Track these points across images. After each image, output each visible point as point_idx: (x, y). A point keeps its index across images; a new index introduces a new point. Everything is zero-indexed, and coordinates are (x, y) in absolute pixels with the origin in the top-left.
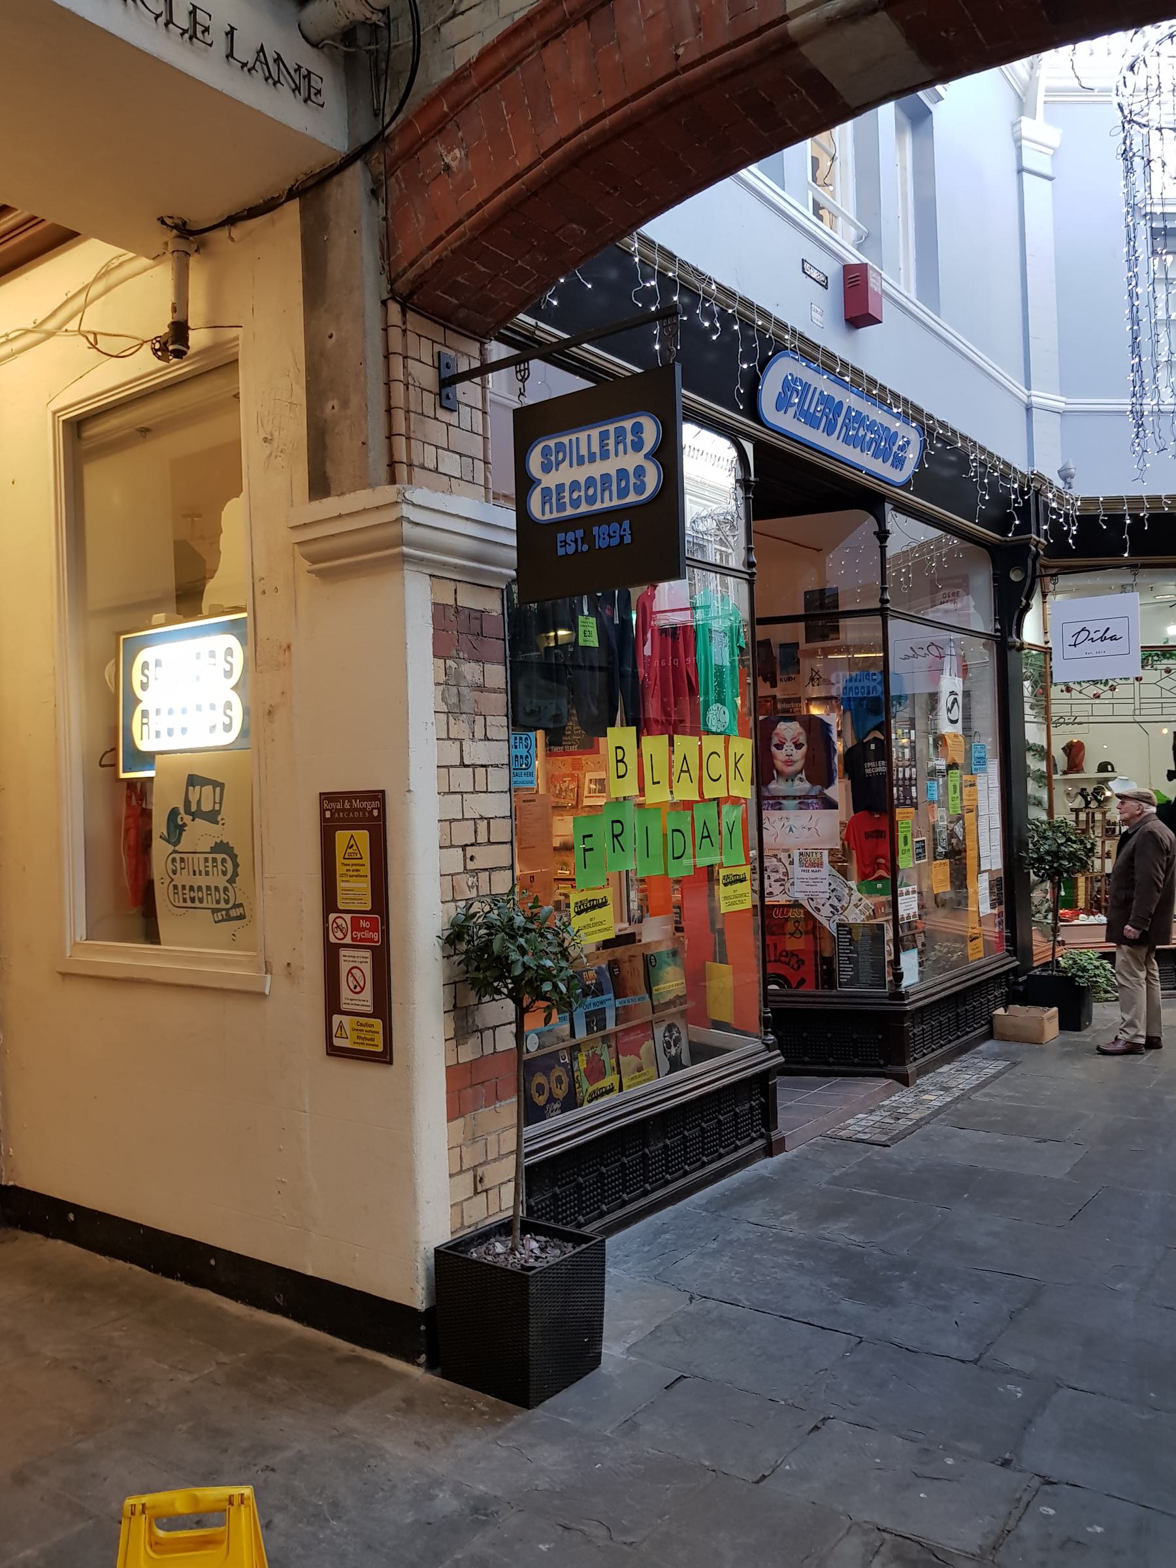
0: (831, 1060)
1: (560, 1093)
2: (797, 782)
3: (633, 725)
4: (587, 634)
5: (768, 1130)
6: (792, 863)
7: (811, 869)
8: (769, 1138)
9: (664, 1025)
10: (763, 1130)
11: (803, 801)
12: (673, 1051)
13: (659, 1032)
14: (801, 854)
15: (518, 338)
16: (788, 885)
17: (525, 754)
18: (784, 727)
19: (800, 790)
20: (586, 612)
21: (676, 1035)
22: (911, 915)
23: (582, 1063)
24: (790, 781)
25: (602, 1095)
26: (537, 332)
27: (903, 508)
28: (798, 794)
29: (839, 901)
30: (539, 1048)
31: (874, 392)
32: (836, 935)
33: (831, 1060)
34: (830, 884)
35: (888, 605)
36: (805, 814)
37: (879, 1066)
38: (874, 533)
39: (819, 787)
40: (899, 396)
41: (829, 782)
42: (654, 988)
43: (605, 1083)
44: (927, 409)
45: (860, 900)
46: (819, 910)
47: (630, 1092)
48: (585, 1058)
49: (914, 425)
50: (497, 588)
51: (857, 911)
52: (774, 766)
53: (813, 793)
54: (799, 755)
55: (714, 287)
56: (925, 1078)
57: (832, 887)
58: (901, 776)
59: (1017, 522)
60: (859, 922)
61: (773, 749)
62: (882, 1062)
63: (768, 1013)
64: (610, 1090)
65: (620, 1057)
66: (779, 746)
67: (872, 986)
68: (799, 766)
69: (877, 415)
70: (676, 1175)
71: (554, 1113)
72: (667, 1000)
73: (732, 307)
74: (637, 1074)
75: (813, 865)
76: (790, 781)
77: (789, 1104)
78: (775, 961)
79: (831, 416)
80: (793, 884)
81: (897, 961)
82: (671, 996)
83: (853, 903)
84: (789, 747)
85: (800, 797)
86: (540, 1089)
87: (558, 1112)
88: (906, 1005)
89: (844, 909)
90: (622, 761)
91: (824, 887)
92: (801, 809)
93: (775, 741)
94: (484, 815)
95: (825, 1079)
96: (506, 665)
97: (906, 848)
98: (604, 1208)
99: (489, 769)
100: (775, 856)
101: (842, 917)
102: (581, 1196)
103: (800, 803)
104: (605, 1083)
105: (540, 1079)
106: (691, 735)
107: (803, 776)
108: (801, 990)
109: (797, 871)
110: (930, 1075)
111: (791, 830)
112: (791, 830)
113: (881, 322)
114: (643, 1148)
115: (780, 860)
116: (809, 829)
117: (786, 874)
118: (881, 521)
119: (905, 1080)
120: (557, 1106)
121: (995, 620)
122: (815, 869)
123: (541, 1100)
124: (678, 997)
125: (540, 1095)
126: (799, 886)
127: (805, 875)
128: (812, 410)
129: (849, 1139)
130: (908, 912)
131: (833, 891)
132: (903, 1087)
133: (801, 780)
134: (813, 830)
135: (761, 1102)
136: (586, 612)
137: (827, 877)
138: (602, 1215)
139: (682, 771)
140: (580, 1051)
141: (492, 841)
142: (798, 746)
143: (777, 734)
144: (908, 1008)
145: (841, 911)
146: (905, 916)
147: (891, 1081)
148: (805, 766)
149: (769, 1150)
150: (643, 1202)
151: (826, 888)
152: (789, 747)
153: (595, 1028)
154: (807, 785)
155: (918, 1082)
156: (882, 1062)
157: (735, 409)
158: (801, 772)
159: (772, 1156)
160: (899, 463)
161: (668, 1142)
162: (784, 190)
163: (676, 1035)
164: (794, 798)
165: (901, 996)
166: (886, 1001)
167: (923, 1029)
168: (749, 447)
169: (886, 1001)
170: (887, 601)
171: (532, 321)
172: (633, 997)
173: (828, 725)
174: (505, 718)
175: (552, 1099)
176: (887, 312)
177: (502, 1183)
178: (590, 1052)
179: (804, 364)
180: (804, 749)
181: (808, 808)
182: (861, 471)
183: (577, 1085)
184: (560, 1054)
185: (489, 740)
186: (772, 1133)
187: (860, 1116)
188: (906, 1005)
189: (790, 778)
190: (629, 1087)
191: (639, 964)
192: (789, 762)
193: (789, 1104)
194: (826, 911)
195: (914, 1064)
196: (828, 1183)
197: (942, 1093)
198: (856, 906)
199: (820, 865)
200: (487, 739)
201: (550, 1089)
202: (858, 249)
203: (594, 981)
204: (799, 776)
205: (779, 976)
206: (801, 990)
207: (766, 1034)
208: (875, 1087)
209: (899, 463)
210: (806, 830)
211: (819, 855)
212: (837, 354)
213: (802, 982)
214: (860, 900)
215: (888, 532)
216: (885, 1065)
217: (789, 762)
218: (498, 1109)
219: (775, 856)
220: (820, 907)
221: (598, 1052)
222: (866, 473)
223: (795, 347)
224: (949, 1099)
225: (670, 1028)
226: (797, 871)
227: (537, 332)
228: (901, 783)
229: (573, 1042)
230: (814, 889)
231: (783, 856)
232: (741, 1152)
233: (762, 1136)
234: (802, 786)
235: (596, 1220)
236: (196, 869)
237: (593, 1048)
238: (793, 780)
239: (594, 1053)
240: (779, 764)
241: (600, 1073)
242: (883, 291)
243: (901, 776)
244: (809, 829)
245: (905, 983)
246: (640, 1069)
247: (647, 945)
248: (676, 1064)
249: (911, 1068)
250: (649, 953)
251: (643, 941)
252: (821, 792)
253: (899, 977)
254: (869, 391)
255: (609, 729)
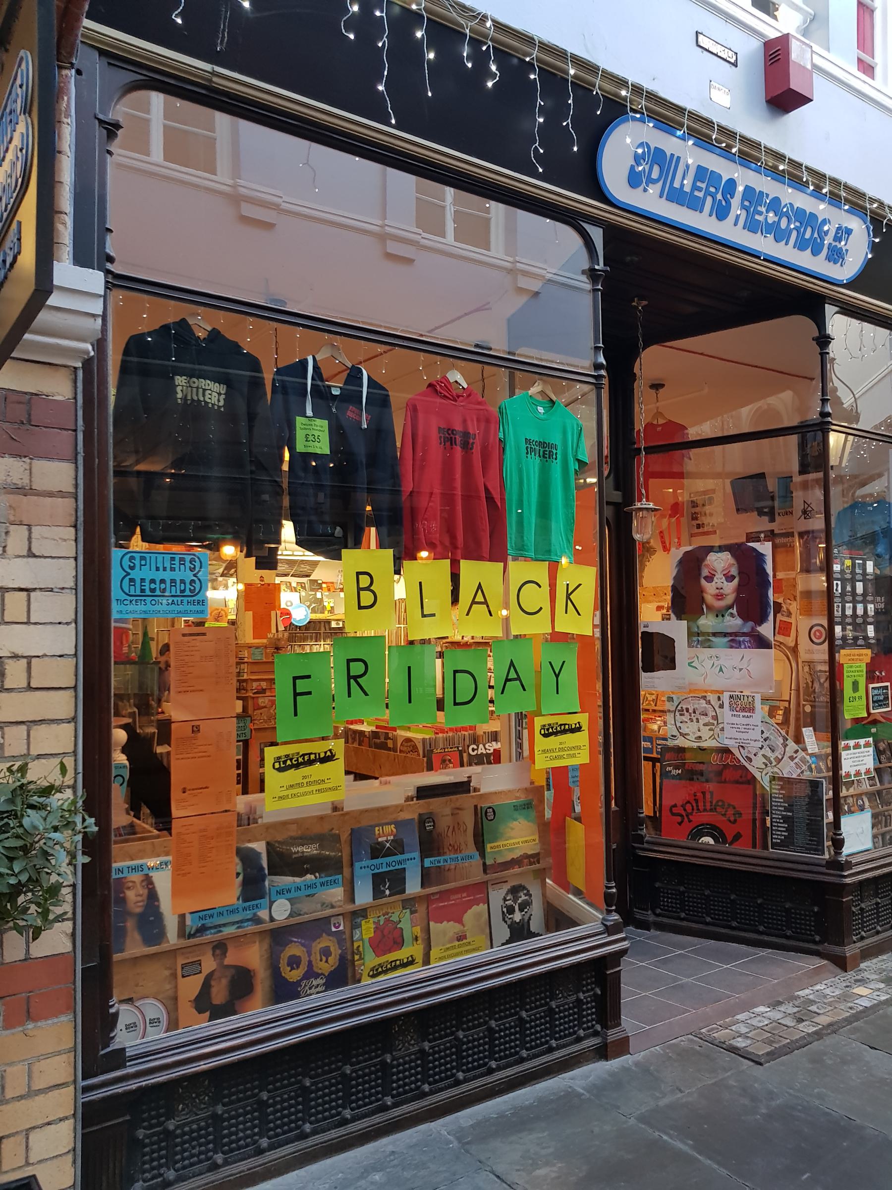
0: (761, 928)
1: (325, 967)
2: (727, 618)
3: (390, 548)
4: (311, 438)
5: (605, 1026)
6: (721, 706)
7: (742, 714)
8: (605, 1037)
9: (506, 887)
10: (598, 1027)
11: (734, 639)
12: (517, 917)
13: (497, 896)
14: (731, 697)
15: (172, 82)
16: (717, 730)
17: (189, 576)
18: (714, 558)
19: (731, 626)
20: (309, 412)
21: (524, 898)
22: (863, 771)
23: (367, 930)
24: (720, 617)
25: (395, 968)
26: (215, 79)
27: (850, 310)
28: (729, 631)
29: (773, 751)
30: (291, 915)
31: (781, 167)
32: (768, 789)
33: (761, 928)
34: (762, 732)
35: (829, 419)
36: (737, 653)
37: (815, 942)
38: (583, 272)
39: (750, 624)
40: (824, 176)
41: (761, 619)
42: (488, 847)
43: (402, 954)
44: (870, 192)
45: (796, 752)
46: (750, 760)
47: (437, 966)
48: (373, 926)
49: (846, 207)
50: (65, 366)
51: (792, 764)
52: (703, 600)
53: (745, 630)
54: (730, 588)
55: (489, 24)
56: (875, 961)
57: (765, 736)
58: (849, 612)
59: (381, 88)
60: (794, 776)
61: (703, 582)
62: (817, 938)
63: (611, 888)
64: (411, 962)
65: (432, 924)
66: (710, 579)
67: (808, 850)
68: (730, 599)
69: (790, 196)
70: (441, 1085)
71: (313, 990)
72: (509, 859)
73: (530, 55)
74: (457, 943)
75: (743, 710)
76: (720, 617)
77: (685, 980)
78: (711, 810)
79: (719, 196)
80: (722, 729)
81: (836, 824)
82: (516, 854)
83: (788, 754)
84: (719, 579)
85: (730, 634)
86: (294, 962)
87: (319, 989)
88: (845, 877)
89: (779, 761)
90: (368, 589)
91: (756, 734)
92: (732, 647)
93: (705, 572)
94: (17, 652)
95: (751, 949)
96: (76, 463)
97: (857, 695)
98: (461, 1075)
99: (33, 594)
100: (704, 698)
101: (776, 770)
102: (863, 917)
103: (731, 641)
104: (402, 954)
105: (295, 949)
106: (491, 560)
107: (734, 611)
108: (735, 848)
109: (726, 715)
110: (884, 957)
111: (721, 670)
112: (721, 670)
113: (812, 100)
114: (383, 1054)
115: (709, 702)
116: (741, 670)
117: (716, 718)
118: (821, 323)
119: (842, 964)
120: (320, 981)
121: (597, 349)
122: (746, 714)
123: (293, 975)
124: (527, 856)
125: (292, 969)
126: (729, 732)
127: (735, 720)
128: (687, 189)
129: (721, 1045)
130: (858, 768)
131: (765, 740)
132: (838, 970)
133: (732, 615)
134: (744, 671)
135: (595, 995)
136: (309, 412)
137: (760, 724)
138: (304, 1136)
139: (474, 602)
140: (365, 917)
141: (33, 685)
142: (730, 578)
143: (707, 566)
144: (848, 881)
145: (774, 763)
146: (853, 773)
147: (826, 962)
148: (738, 601)
149: (603, 1053)
150: (377, 1119)
151: (758, 736)
152: (719, 579)
153: (387, 892)
154: (738, 621)
155: (862, 965)
156: (817, 938)
157: (534, 174)
158: (731, 607)
159: (607, 1059)
160: (836, 256)
161: (581, 996)
162: (828, 50)
163: (524, 898)
164: (725, 635)
165: (836, 865)
166: (824, 870)
167: (877, 904)
168: (597, 234)
169: (824, 870)
170: (828, 415)
171: (207, 67)
172: (453, 856)
173: (763, 555)
174: (73, 530)
175: (311, 973)
176: (820, 89)
177: (34, 1128)
178: (382, 919)
179: (651, 125)
180: (736, 581)
181: (739, 647)
182: (759, 258)
183: (357, 957)
184: (333, 920)
185: (35, 556)
186: (610, 1032)
187: (762, 1009)
188: (845, 877)
189: (720, 613)
190: (441, 959)
191: (469, 820)
192: (720, 596)
193: (685, 980)
194: (759, 761)
195: (859, 945)
196: (642, 1119)
197: (882, 985)
198: (792, 758)
199: (752, 709)
200: (31, 555)
201: (310, 962)
202: (803, 35)
203: (392, 837)
204: (731, 611)
205: (714, 827)
206: (735, 848)
207: (609, 912)
208: (800, 968)
209: (836, 256)
210: (736, 671)
211: (750, 699)
212: (715, 121)
213: (737, 837)
214: (796, 752)
215: (829, 337)
216: (820, 942)
217: (720, 596)
218: (30, 1033)
219: (704, 698)
220: (752, 756)
221: (395, 918)
222: (764, 260)
223: (642, 108)
224: (883, 998)
225: (515, 891)
226: (726, 715)
227: (215, 79)
228: (849, 620)
229: (350, 907)
230: (744, 736)
231: (712, 697)
232: (557, 1054)
233: (596, 1034)
234: (733, 622)
235: (292, 1142)
236: (160, 566)
237: (387, 914)
238: (723, 616)
239: (387, 921)
240: (709, 598)
241: (395, 942)
242: (814, 66)
243: (849, 612)
244: (741, 670)
245: (846, 850)
246: (461, 938)
247: (483, 796)
248: (520, 932)
249: (850, 950)
250: (486, 805)
251: (482, 792)
252: (753, 629)
253: (838, 844)
254: (776, 168)
255: (343, 551)
